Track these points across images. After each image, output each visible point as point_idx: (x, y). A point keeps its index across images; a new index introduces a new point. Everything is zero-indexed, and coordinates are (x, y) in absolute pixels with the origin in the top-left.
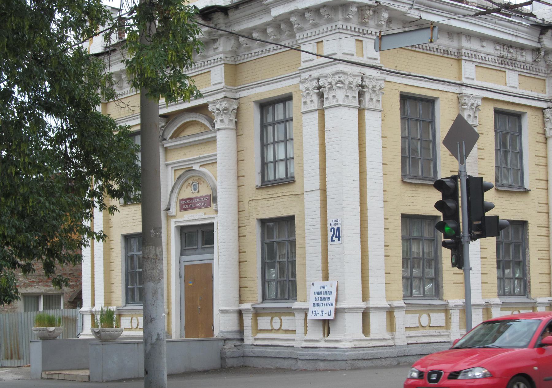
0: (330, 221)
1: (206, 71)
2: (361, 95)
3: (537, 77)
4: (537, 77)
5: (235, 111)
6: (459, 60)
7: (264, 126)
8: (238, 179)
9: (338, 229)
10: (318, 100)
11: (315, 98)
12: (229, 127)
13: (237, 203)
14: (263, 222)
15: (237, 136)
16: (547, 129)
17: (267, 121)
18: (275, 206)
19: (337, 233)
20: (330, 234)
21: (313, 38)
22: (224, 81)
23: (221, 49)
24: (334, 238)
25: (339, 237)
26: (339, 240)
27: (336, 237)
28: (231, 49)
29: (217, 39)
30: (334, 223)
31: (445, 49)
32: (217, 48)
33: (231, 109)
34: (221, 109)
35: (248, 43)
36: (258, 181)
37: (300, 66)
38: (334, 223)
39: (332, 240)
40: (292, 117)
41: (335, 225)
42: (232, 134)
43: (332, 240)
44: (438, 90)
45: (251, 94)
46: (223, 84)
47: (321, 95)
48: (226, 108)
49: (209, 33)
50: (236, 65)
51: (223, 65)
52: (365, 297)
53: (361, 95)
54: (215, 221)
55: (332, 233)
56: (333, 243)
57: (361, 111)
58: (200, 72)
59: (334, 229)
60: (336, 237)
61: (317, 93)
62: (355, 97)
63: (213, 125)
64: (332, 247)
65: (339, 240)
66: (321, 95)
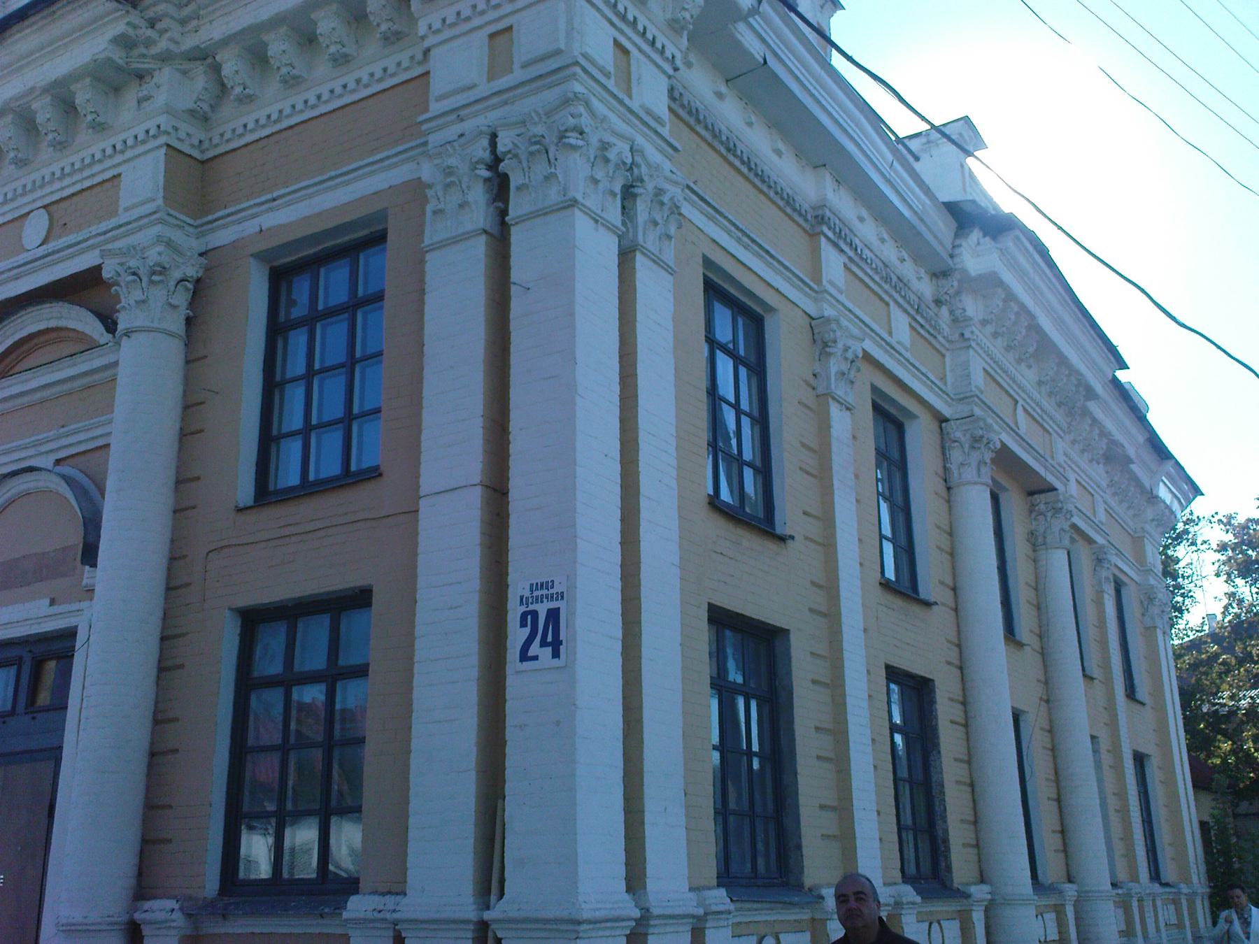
0: (518, 586)
1: (109, 174)
2: (628, 194)
3: (933, 341)
4: (933, 341)
5: (190, 286)
6: (813, 235)
7: (276, 330)
8: (176, 490)
9: (554, 615)
10: (487, 205)
11: (478, 195)
12: (164, 325)
13: (165, 561)
14: (253, 620)
15: (187, 362)
16: (953, 467)
17: (284, 372)
18: (296, 560)
19: (550, 631)
20: (517, 635)
21: (477, 22)
22: (161, 194)
23: (161, 99)
24: (535, 649)
25: (556, 648)
26: (556, 654)
27: (544, 643)
28: (192, 106)
29: (150, 73)
30: (539, 593)
31: (790, 193)
32: (148, 98)
33: (177, 275)
34: (141, 272)
35: (248, 82)
36: (245, 490)
37: (426, 110)
38: (539, 593)
39: (524, 657)
40: (383, 291)
41: (539, 600)
42: (173, 351)
43: (524, 657)
44: (777, 290)
45: (245, 234)
46: (160, 202)
47: (500, 188)
48: (159, 264)
49: (125, 42)
50: (203, 162)
51: (163, 150)
52: (490, 877)
53: (628, 194)
54: (81, 623)
55: (527, 630)
56: (528, 665)
57: (626, 256)
58: (87, 184)
59: (535, 614)
60: (544, 643)
61: (487, 180)
62: (614, 194)
63: (110, 325)
64: (522, 683)
65: (556, 654)
66: (500, 188)
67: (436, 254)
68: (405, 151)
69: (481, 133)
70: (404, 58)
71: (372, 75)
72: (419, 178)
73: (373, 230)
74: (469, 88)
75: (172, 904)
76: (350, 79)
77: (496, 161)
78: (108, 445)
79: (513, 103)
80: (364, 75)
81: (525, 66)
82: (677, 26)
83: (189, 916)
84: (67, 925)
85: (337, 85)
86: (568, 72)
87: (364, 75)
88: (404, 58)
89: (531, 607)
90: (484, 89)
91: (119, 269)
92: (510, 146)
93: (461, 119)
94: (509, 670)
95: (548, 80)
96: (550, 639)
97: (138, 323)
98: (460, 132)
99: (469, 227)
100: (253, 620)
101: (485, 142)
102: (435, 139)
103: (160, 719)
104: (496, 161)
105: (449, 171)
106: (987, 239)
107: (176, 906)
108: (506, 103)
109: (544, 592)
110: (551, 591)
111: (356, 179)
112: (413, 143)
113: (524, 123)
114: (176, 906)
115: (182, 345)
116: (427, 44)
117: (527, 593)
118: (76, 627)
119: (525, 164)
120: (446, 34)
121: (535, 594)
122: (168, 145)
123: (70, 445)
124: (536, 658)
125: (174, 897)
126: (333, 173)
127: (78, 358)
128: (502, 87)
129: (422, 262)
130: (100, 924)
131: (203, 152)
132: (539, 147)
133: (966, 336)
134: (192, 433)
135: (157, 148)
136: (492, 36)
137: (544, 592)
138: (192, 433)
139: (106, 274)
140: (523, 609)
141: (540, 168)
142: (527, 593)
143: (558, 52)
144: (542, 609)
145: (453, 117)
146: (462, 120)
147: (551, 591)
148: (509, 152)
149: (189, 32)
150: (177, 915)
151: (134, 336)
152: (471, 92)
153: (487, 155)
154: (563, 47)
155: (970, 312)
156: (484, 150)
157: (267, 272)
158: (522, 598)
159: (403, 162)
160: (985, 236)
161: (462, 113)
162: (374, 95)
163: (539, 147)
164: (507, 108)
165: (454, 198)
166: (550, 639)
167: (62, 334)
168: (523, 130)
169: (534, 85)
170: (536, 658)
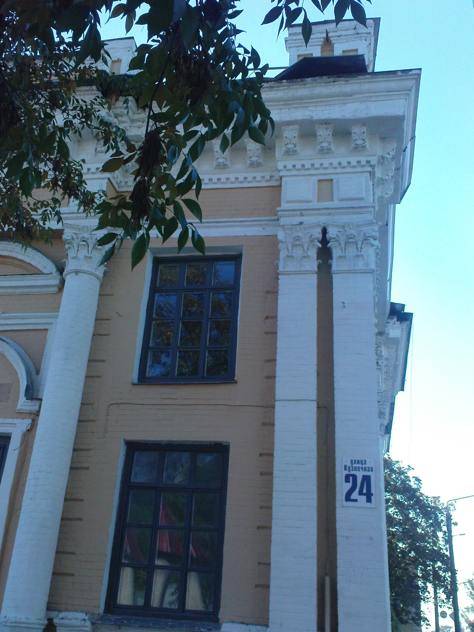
20: (342, 487)
21: (313, 172)
26: (369, 500)
27: (361, 493)
30: (357, 465)
38: (357, 465)
39: (348, 498)
41: (358, 469)
59: (355, 477)
60: (361, 493)
65: (369, 500)
66: (325, 253)
67: (286, 277)
68: (258, 221)
69: (319, 225)
70: (259, 176)
71: (237, 179)
72: (276, 236)
73: (226, 253)
74: (307, 202)
75: (82, 616)
76: (223, 177)
77: (324, 241)
78: (47, 330)
79: (334, 215)
80: (232, 177)
81: (342, 200)
82: (381, 200)
83: (93, 624)
84: (15, 622)
85: (215, 178)
86: (369, 209)
87: (232, 177)
88: (259, 176)
89: (352, 472)
90: (315, 204)
91: (74, 236)
92: (335, 236)
93: (302, 215)
94: (338, 504)
95: (356, 210)
96: (365, 491)
97: (85, 268)
98: (300, 221)
99: (308, 268)
100: (133, 448)
101: (320, 230)
102: (283, 221)
103: (70, 499)
104: (324, 241)
105: (297, 238)
106: (399, 322)
107: (86, 618)
108: (329, 214)
109: (360, 465)
110: (364, 466)
111: (223, 227)
112: (264, 218)
113: (343, 227)
114: (86, 618)
115: (97, 284)
116: (281, 174)
117: (349, 464)
118: (11, 433)
119: (343, 246)
120: (294, 173)
121: (354, 465)
122: (109, 179)
123: (7, 324)
124: (356, 500)
125: (82, 611)
126: (210, 220)
127: (28, 277)
128: (330, 207)
129: (277, 279)
130: (34, 624)
131: (119, 187)
132: (350, 240)
133: (379, 364)
134: (99, 335)
135: (104, 178)
136: (319, 181)
137: (360, 465)
138: (102, 335)
139: (64, 237)
140: (347, 472)
141: (351, 251)
142: (349, 464)
143: (362, 199)
144: (360, 475)
145: (299, 213)
146: (303, 216)
147: (364, 466)
148: (334, 238)
149: (135, 127)
150: (88, 623)
151: (80, 274)
152: (307, 204)
153: (320, 236)
154: (364, 196)
155: (383, 353)
156: (319, 234)
157: (152, 259)
158: (345, 467)
159: (256, 225)
160: (397, 321)
161: (304, 212)
162: (236, 188)
163: (350, 240)
164: (329, 217)
165: (298, 252)
166: (365, 491)
167: (7, 260)
168: (342, 230)
169: (349, 211)
170: (356, 500)
